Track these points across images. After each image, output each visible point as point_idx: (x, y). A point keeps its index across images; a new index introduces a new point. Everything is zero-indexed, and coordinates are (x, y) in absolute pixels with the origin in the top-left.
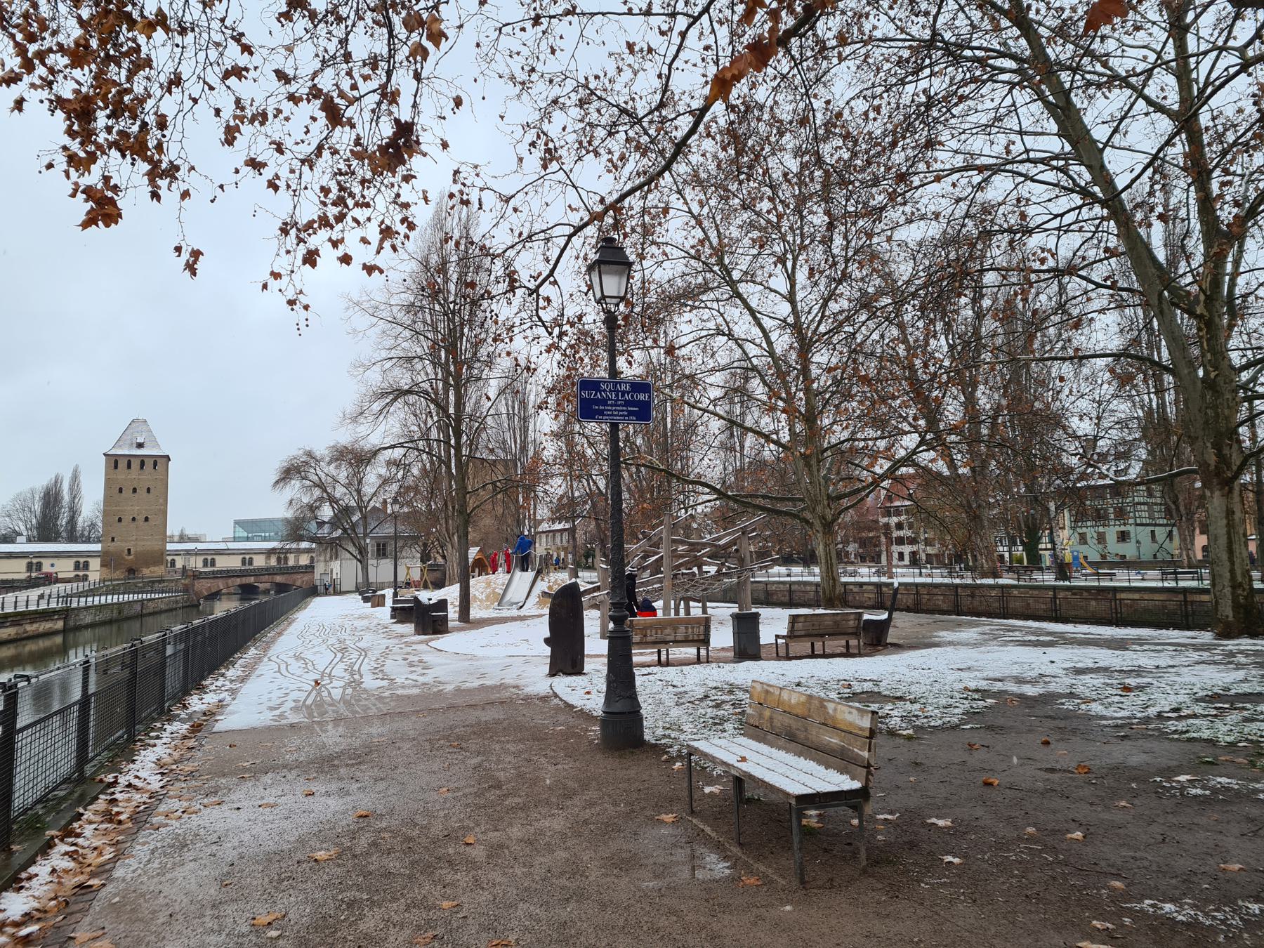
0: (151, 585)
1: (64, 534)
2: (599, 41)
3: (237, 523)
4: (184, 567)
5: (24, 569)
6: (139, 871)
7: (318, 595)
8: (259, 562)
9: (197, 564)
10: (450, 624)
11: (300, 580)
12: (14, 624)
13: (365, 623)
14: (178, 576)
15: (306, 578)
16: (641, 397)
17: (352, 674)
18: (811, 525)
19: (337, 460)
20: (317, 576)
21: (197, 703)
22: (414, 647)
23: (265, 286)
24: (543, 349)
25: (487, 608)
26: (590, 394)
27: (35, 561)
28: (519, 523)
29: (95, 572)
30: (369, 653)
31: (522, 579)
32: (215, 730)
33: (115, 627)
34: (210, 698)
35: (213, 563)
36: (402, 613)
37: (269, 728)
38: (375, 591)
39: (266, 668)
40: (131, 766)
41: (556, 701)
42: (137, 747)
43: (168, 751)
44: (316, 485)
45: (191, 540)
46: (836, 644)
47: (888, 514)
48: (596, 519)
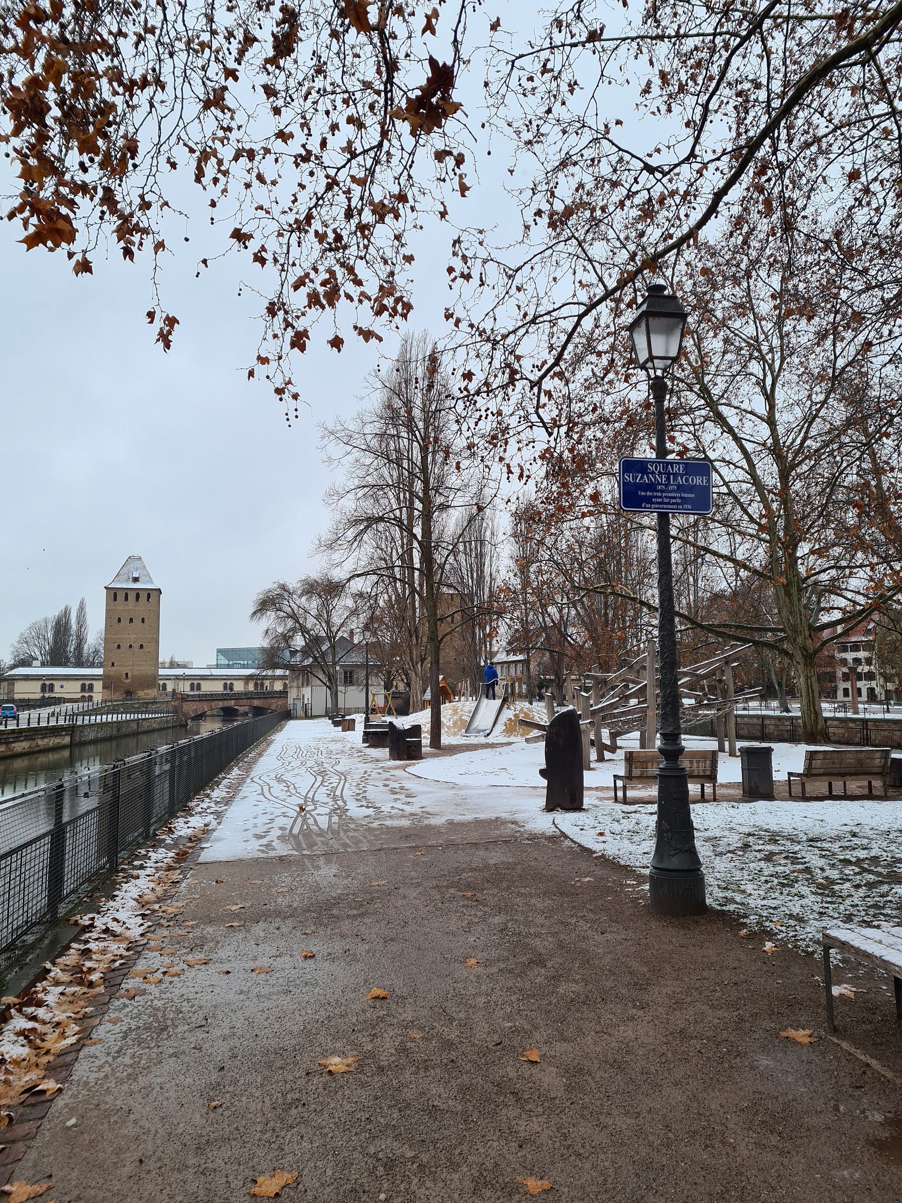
0: (146, 706)
1: (72, 660)
2: (621, 80)
3: (219, 651)
4: (174, 690)
5: (39, 690)
6: (107, 1069)
7: (296, 718)
8: (239, 687)
9: (185, 688)
10: (424, 750)
11: (275, 704)
12: (28, 738)
13: (339, 746)
14: (169, 699)
15: (281, 702)
16: (698, 481)
17: (335, 799)
18: (791, 656)
19: (307, 593)
20: (290, 701)
21: (183, 827)
22: (393, 772)
23: (251, 374)
24: (537, 454)
25: (455, 734)
26: (635, 478)
27: (48, 683)
28: (477, 654)
29: (98, 694)
30: (349, 777)
31: (490, 707)
32: (201, 860)
33: (114, 744)
34: (196, 822)
35: (199, 687)
36: (373, 738)
37: (256, 861)
38: (343, 716)
39: (249, 790)
40: (111, 903)
41: (567, 843)
42: (119, 879)
43: (152, 885)
44: (289, 616)
45: (179, 666)
46: (854, 786)
47: (845, 650)
48: (551, 652)
